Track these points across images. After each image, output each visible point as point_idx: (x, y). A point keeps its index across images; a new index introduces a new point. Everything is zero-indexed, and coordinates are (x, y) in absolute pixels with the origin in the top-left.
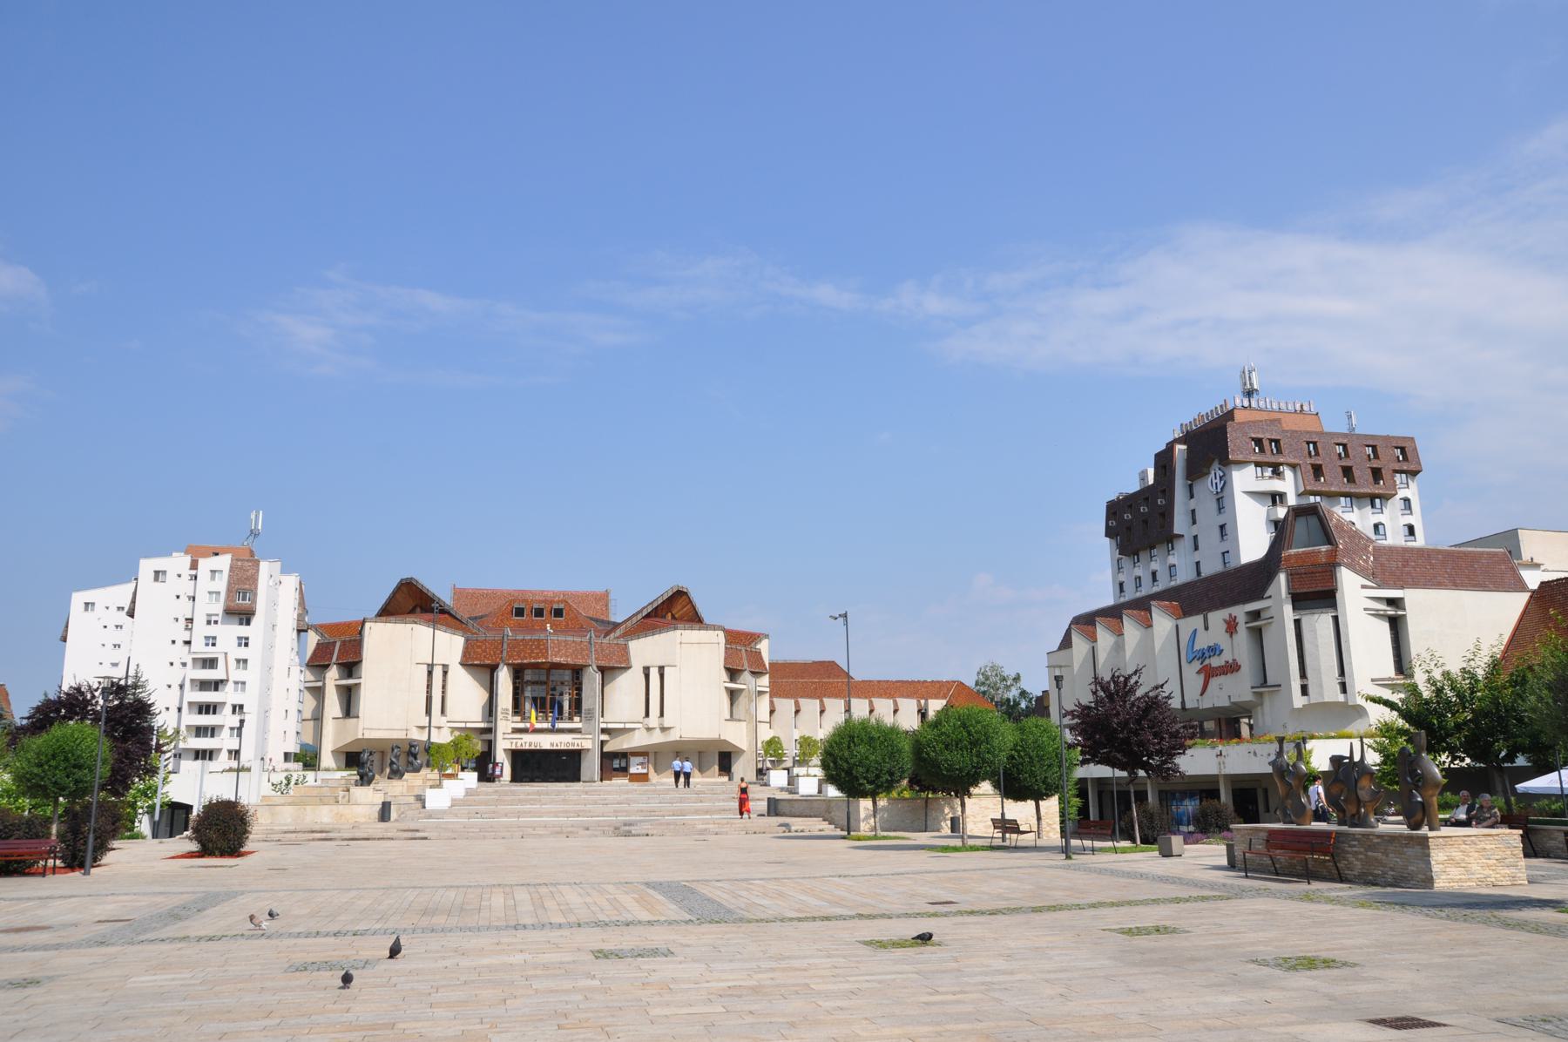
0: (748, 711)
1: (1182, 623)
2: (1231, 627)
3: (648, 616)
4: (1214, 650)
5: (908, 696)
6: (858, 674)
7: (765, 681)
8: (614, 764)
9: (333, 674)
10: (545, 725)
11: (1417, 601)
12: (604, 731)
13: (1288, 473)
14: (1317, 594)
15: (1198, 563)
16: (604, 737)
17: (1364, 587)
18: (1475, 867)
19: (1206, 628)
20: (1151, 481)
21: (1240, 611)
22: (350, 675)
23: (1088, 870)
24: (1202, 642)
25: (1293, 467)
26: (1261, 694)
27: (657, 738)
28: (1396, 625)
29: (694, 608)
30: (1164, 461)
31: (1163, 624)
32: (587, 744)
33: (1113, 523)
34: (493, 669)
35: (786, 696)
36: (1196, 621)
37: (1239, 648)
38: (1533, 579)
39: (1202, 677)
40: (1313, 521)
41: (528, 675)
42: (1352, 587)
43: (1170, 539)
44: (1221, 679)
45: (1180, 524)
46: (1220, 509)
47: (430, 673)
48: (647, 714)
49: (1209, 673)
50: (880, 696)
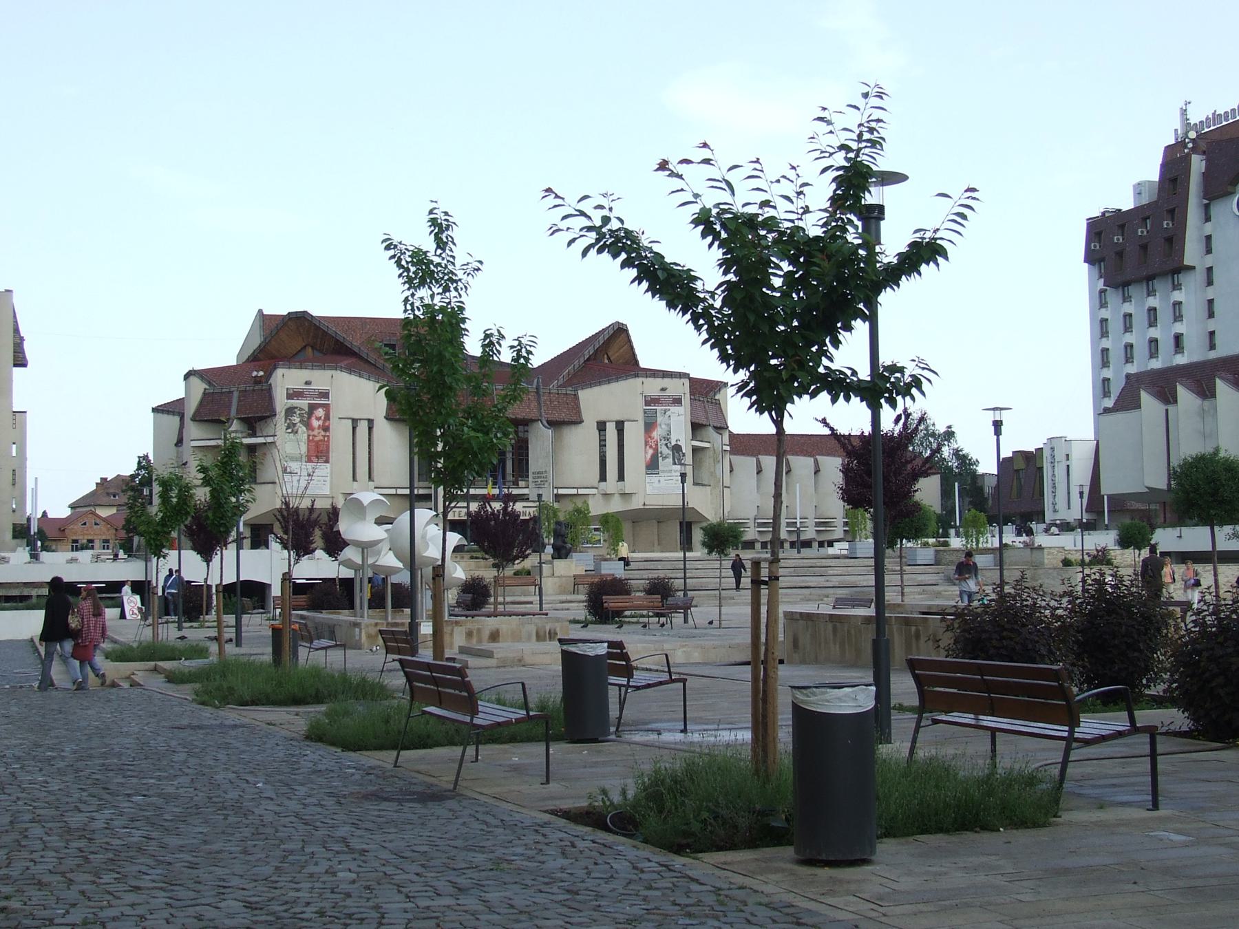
0: (713, 474)
10: (1171, 608)
27: (616, 506)
29: (632, 348)
43: (1176, 270)
45: (1192, 253)
48: (603, 478)
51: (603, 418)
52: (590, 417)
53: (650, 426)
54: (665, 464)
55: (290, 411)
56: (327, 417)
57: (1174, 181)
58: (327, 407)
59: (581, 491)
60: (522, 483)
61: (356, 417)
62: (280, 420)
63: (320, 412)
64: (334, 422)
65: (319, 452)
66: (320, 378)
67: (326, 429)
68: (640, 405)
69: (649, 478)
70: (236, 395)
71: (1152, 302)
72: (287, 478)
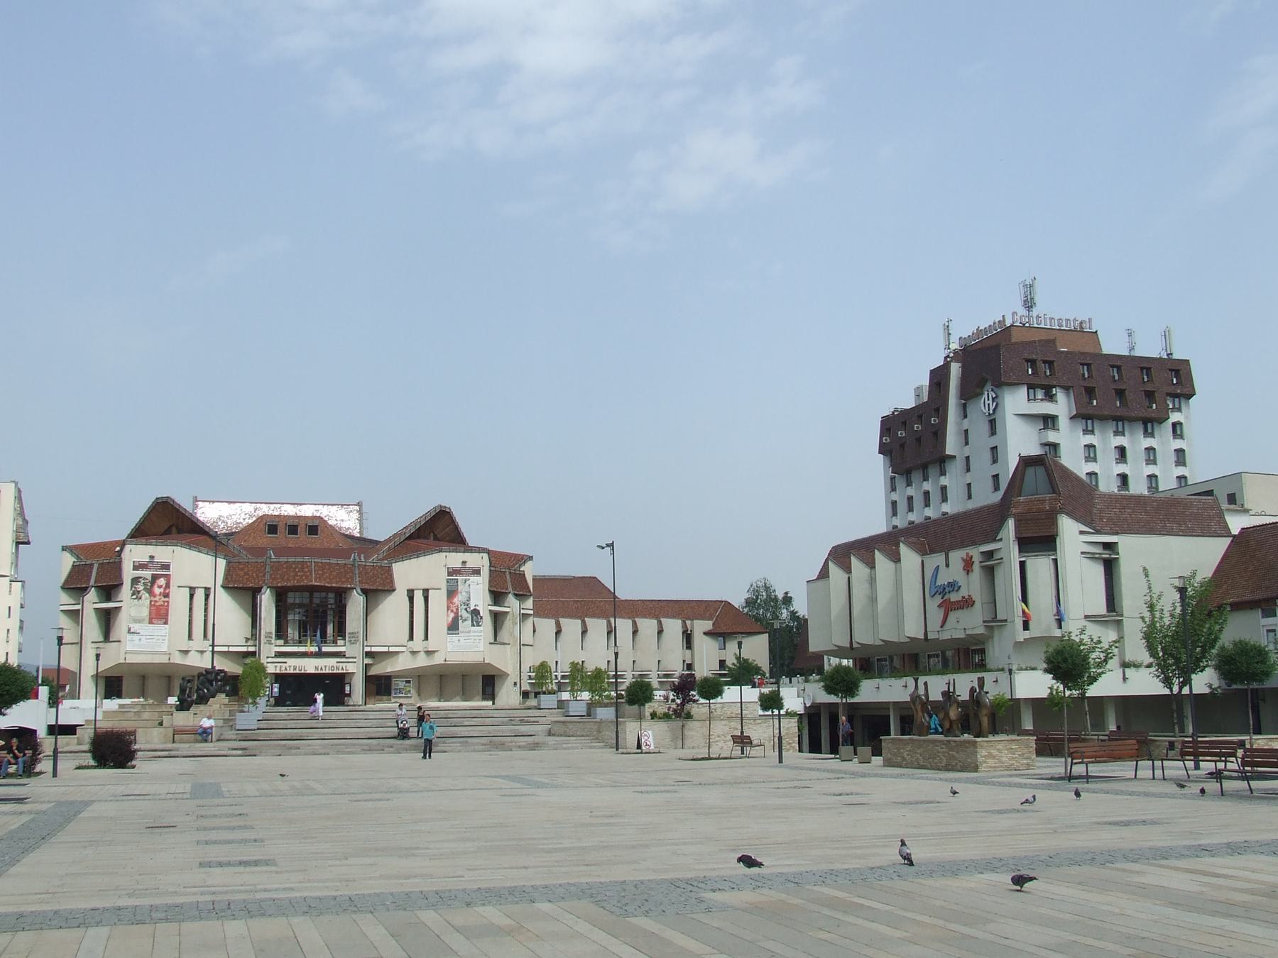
0: (511, 634)
1: (927, 559)
2: (968, 565)
3: (410, 537)
4: (953, 586)
5: (673, 617)
6: (622, 594)
7: (529, 603)
8: (379, 686)
9: (92, 596)
11: (1127, 544)
12: (368, 654)
13: (1060, 396)
14: (1040, 540)
15: (969, 485)
16: (367, 661)
17: (1082, 532)
18: (1004, 759)
19: (947, 565)
20: (926, 399)
21: (976, 552)
22: (108, 599)
23: (1112, 869)
24: (943, 580)
25: (1066, 389)
26: (992, 627)
27: (422, 661)
28: (1110, 567)
30: (939, 378)
31: (910, 557)
32: (351, 668)
33: (887, 440)
34: (256, 591)
35: (547, 616)
36: (938, 559)
37: (973, 585)
38: (1236, 523)
39: (942, 610)
40: (1040, 470)
41: (292, 598)
42: (1070, 531)
43: (942, 461)
44: (959, 613)
45: (952, 445)
46: (993, 432)
47: (192, 596)
48: (411, 638)
49: (948, 607)
50: (645, 616)
51: (411, 587)
52: (401, 584)
53: (451, 593)
54: (464, 626)
55: (135, 581)
56: (168, 586)
57: (939, 384)
58: (168, 577)
59: (392, 649)
60: (340, 642)
61: (194, 585)
62: (126, 590)
63: (162, 581)
64: (173, 590)
65: (159, 614)
66: (163, 553)
67: (167, 595)
68: (444, 575)
69: (450, 638)
70: (96, 567)
71: (927, 486)
72: (129, 637)
